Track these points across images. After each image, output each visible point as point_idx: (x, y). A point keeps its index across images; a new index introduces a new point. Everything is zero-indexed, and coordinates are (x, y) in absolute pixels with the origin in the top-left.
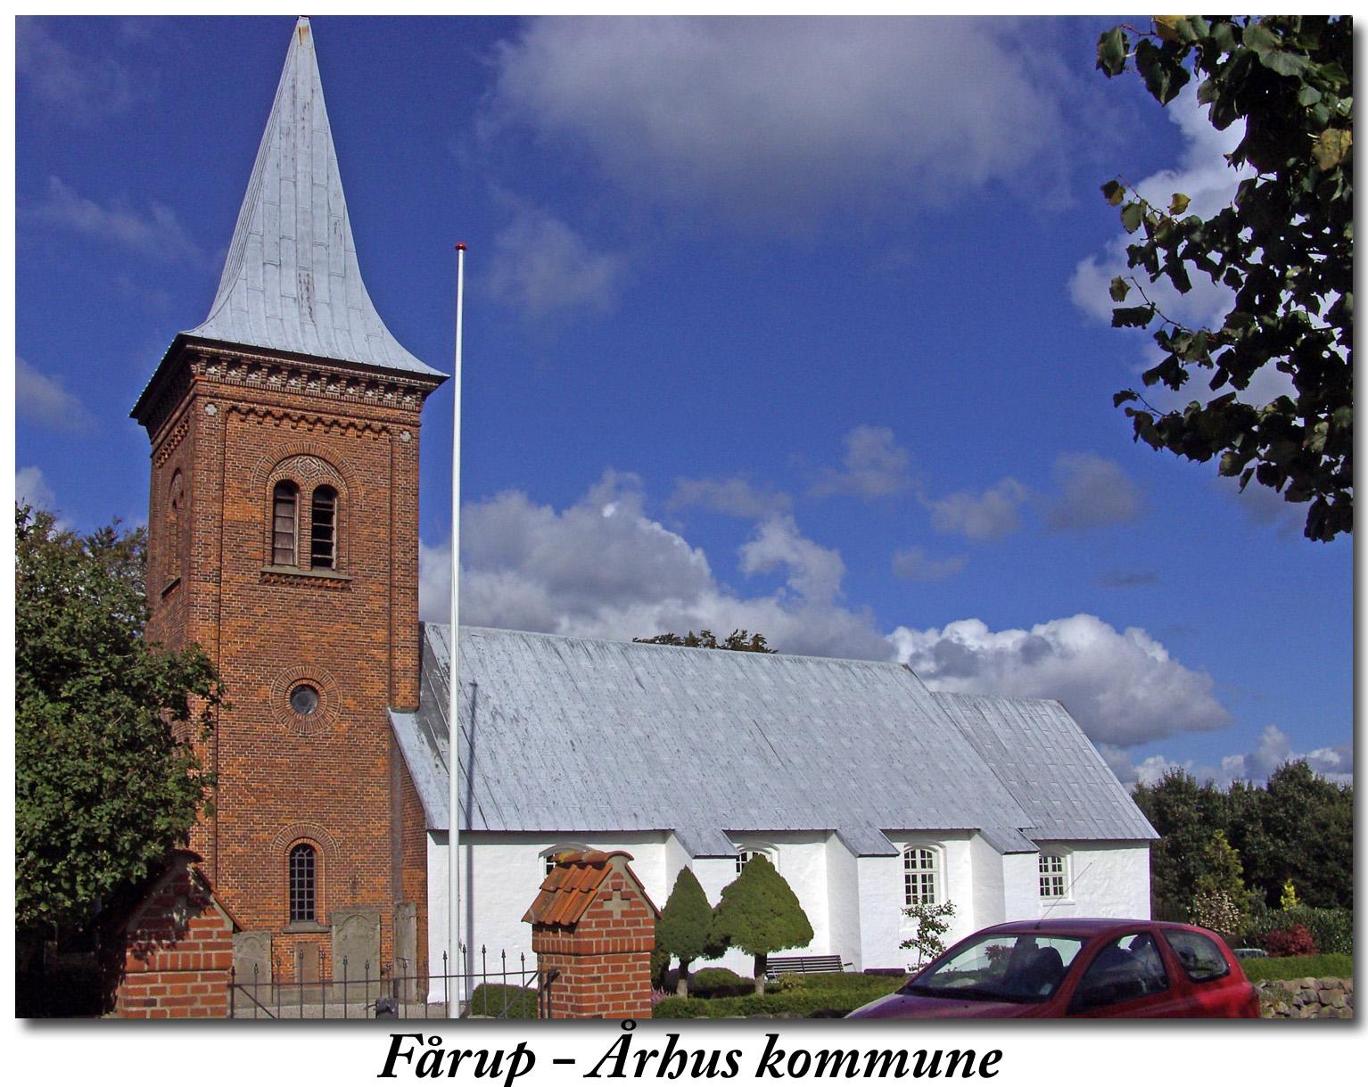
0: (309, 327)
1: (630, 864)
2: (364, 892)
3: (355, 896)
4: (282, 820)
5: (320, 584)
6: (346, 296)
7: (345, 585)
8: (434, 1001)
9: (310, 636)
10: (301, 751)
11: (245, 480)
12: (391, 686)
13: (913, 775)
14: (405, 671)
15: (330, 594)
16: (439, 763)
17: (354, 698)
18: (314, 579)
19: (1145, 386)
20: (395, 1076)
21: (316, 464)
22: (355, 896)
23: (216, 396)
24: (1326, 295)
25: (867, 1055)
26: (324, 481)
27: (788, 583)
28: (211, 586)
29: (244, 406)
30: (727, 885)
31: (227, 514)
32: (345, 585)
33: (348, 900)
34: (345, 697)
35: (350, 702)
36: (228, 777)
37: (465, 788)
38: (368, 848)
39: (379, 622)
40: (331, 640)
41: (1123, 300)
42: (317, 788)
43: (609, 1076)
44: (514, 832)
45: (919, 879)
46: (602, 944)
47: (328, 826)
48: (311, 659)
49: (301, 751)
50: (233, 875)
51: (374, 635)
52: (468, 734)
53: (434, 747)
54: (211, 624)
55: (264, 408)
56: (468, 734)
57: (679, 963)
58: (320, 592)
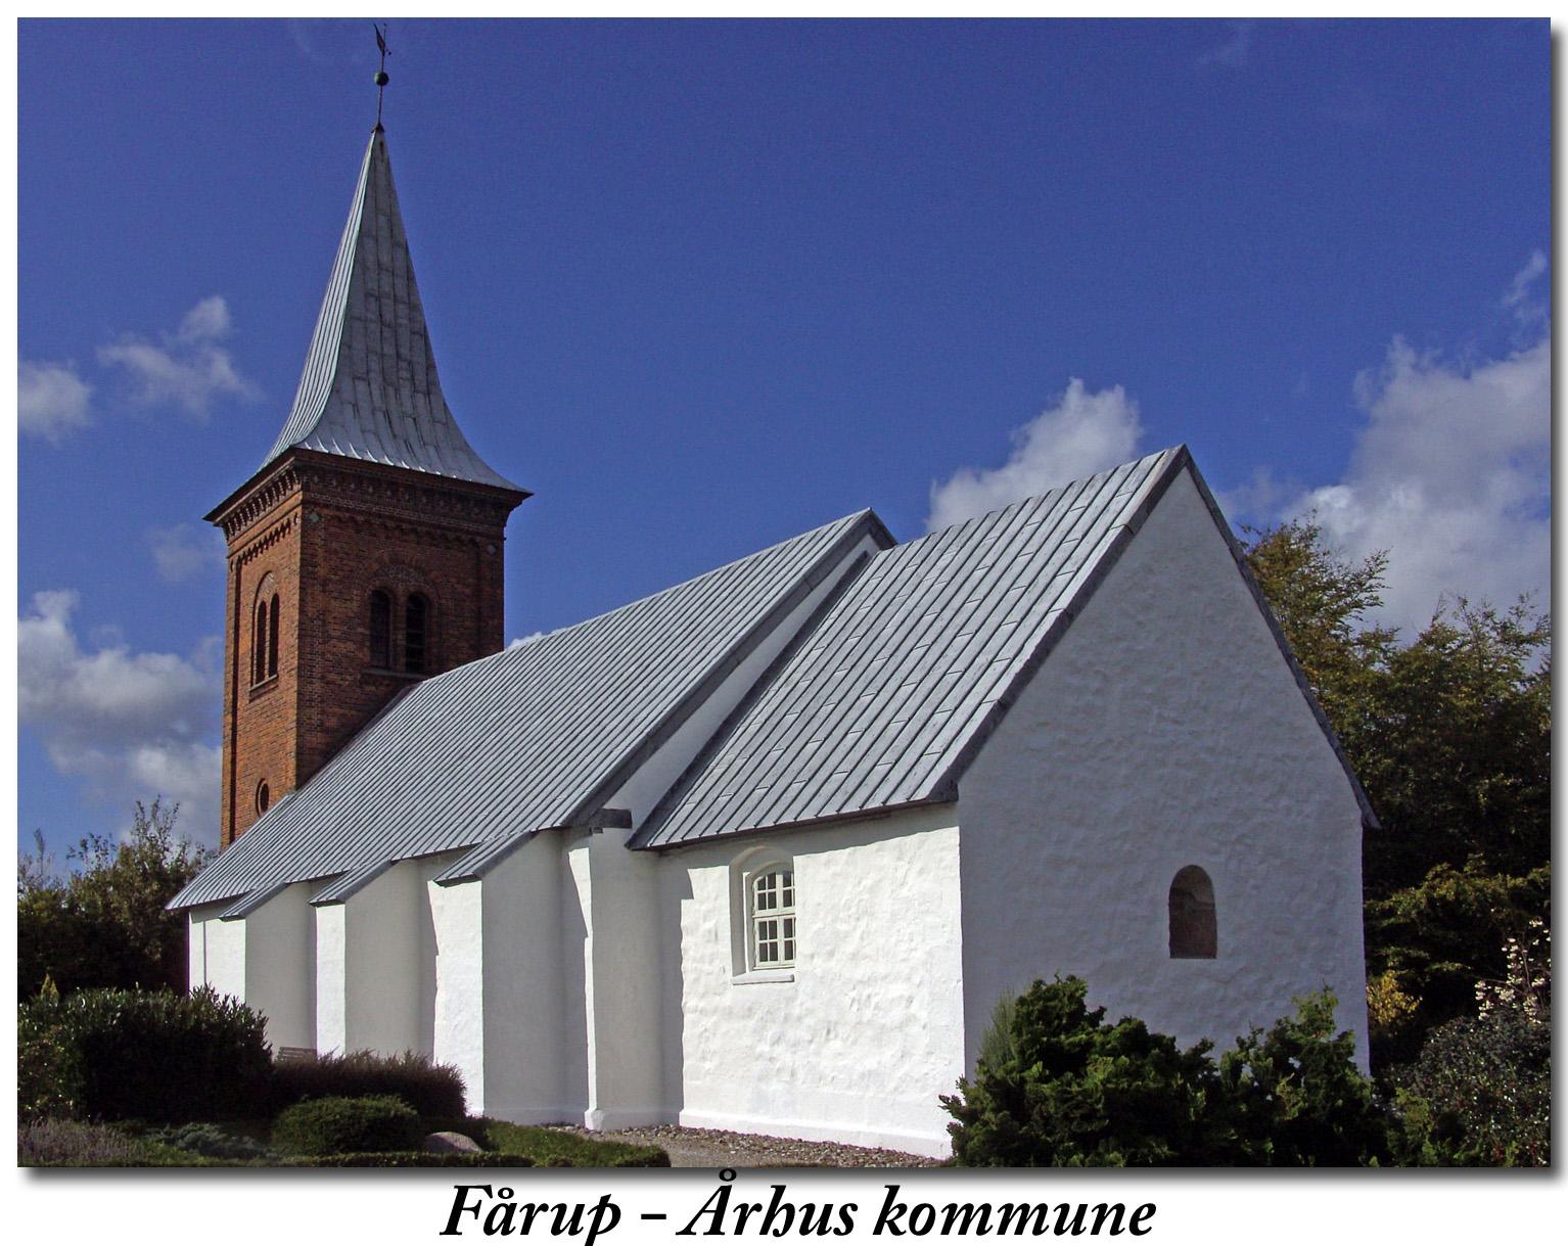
20: (460, 1234)
29: (360, 518)
43: (705, 1234)
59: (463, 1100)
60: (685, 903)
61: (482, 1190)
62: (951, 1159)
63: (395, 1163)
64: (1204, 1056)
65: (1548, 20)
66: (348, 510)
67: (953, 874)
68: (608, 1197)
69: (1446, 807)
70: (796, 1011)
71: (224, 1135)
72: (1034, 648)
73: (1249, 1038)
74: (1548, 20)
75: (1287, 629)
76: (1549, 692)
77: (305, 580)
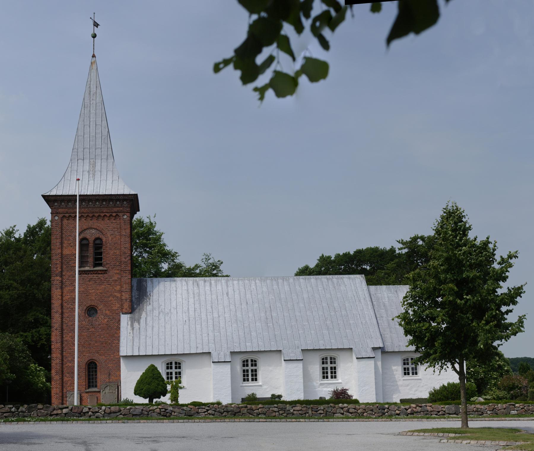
0: (91, 182)
1: (282, 399)
2: (113, 377)
3: (109, 379)
4: (84, 354)
5: (97, 272)
6: (228, 412)
7: (105, 272)
8: (191, 280)
9: (93, 291)
10: (90, 330)
11: (69, 240)
12: (122, 305)
13: (112, 223)
14: (126, 300)
15: (100, 275)
16: (131, 332)
17: (109, 310)
18: (198, 291)
19: (240, 83)
20: (217, 68)
21: (93, 231)
22: (109, 379)
23: (57, 213)
24: (394, 297)
25: (155, 223)
26: (97, 236)
27: (504, 311)
28: (58, 278)
29: (67, 215)
30: (381, 247)
31: (64, 253)
32: (105, 272)
33: (107, 380)
34: (106, 310)
35: (107, 312)
36: (66, 341)
37: (66, 338)
38: (114, 362)
39: (117, 283)
40: (100, 291)
41: (135, 394)
42: (96, 342)
43: (305, 272)
44: (375, 379)
45: (329, 369)
46: (91, 260)
47: (100, 355)
48: (94, 299)
49: (90, 330)
50: (68, 373)
51: (115, 288)
52: (94, 71)
53: (132, 325)
54: (59, 290)
55: (86, 214)
56: (94, 71)
57: (356, 6)
58: (96, 275)
59: (440, 388)
60: (368, 6)
61: (428, 369)
62: (253, 28)
63: (513, 412)
64: (448, 376)
65: (139, 211)
66: (67, 213)
67: (326, 280)
68: (398, 31)
69: (10, 408)
70: (422, 385)
71: (448, 376)
72: (139, 377)
73: (444, 212)
74: (139, 211)
75: (39, 241)
76: (170, 416)
77: (72, 388)
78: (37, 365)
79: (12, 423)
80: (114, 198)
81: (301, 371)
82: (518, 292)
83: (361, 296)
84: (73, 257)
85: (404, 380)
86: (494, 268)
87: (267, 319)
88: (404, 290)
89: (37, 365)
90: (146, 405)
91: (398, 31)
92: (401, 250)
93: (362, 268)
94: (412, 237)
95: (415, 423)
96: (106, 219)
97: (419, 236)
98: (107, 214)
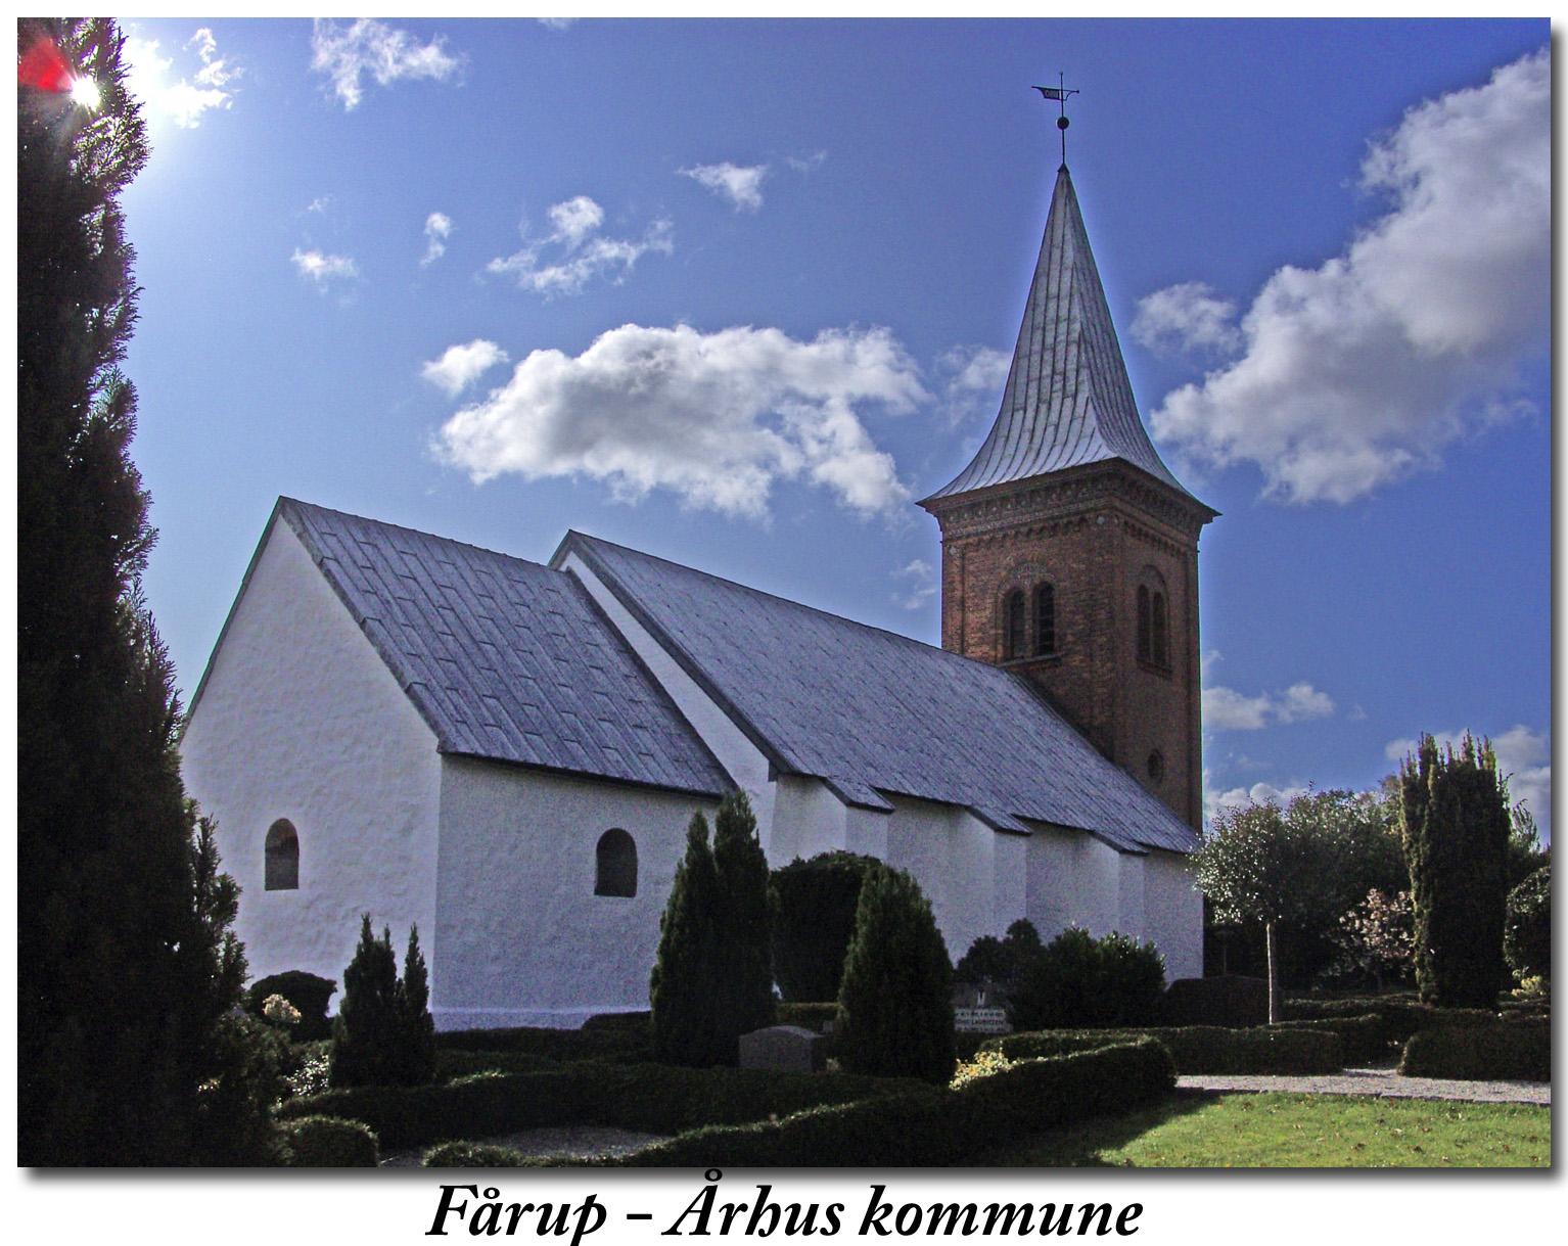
20: (446, 1234)
43: (690, 1234)
59: (939, 931)
63: (439, 971)
65: (1548, 20)
68: (594, 1196)
74: (1548, 20)
78: (1402, 894)
79: (250, 586)
80: (1008, 492)
81: (830, 794)
82: (373, 961)
83: (494, 658)
84: (1208, 972)
85: (511, 1230)
86: (230, 1027)
87: (735, 688)
88: (1176, 1086)
89: (1402, 894)
90: (560, 565)
91: (594, 1196)
92: (493, 393)
93: (819, 1029)
94: (210, 104)
95: (420, 717)
96: (1046, 533)
97: (126, 83)
98: (1073, 519)
